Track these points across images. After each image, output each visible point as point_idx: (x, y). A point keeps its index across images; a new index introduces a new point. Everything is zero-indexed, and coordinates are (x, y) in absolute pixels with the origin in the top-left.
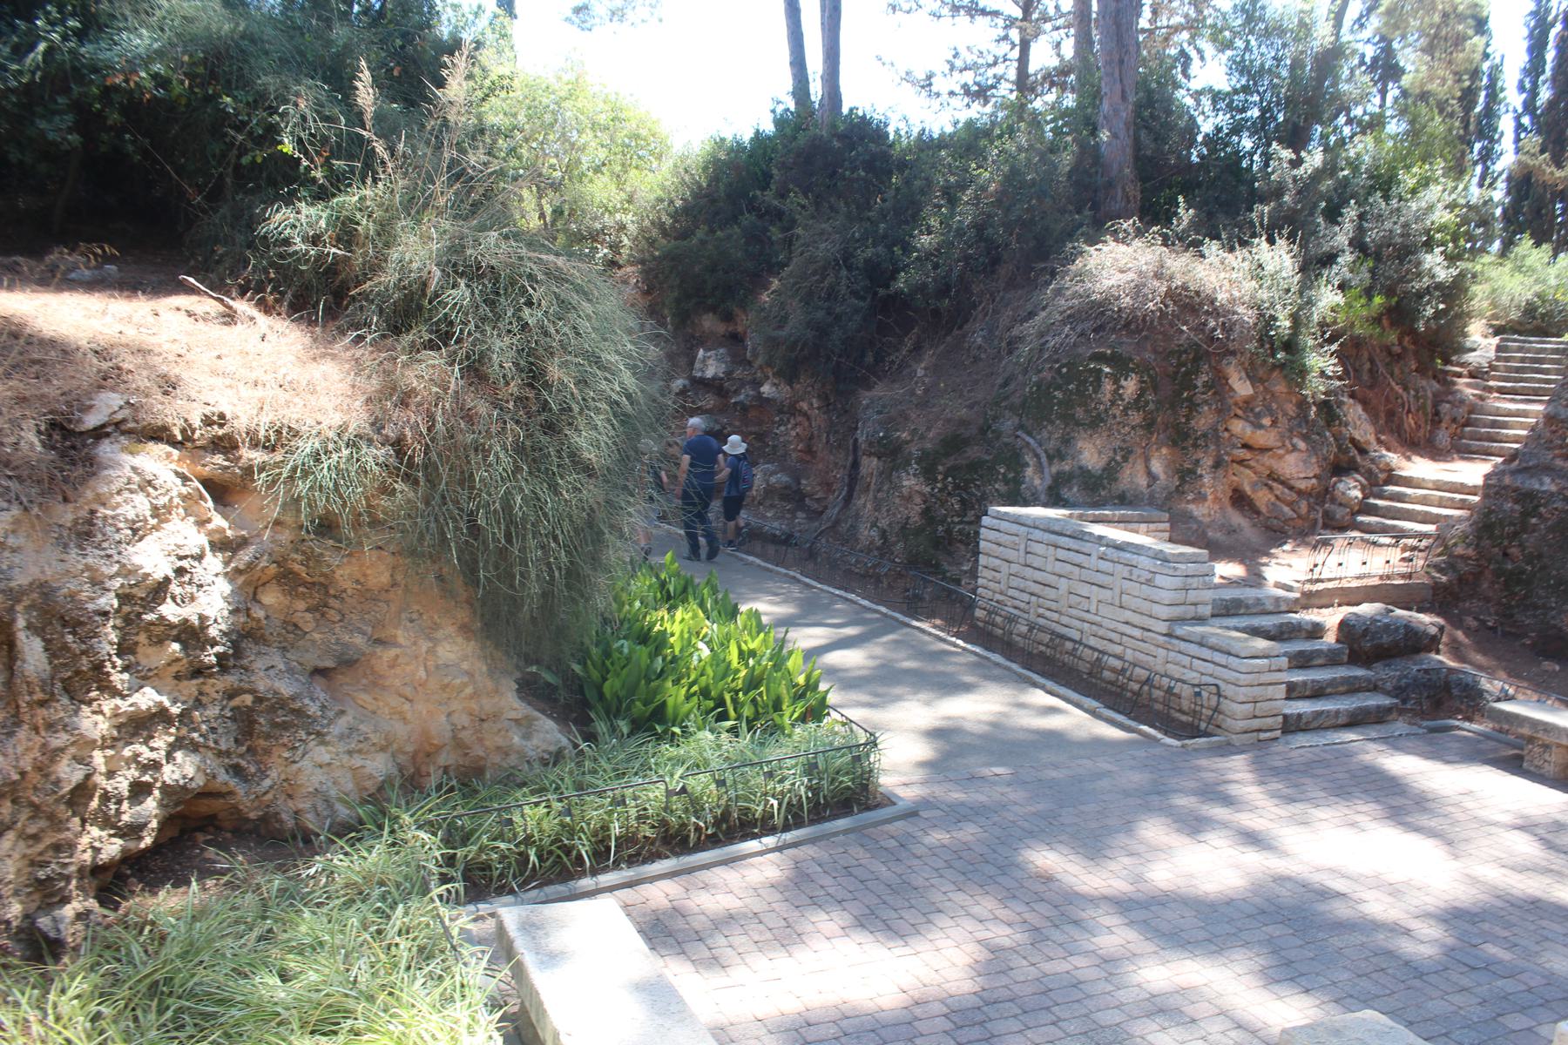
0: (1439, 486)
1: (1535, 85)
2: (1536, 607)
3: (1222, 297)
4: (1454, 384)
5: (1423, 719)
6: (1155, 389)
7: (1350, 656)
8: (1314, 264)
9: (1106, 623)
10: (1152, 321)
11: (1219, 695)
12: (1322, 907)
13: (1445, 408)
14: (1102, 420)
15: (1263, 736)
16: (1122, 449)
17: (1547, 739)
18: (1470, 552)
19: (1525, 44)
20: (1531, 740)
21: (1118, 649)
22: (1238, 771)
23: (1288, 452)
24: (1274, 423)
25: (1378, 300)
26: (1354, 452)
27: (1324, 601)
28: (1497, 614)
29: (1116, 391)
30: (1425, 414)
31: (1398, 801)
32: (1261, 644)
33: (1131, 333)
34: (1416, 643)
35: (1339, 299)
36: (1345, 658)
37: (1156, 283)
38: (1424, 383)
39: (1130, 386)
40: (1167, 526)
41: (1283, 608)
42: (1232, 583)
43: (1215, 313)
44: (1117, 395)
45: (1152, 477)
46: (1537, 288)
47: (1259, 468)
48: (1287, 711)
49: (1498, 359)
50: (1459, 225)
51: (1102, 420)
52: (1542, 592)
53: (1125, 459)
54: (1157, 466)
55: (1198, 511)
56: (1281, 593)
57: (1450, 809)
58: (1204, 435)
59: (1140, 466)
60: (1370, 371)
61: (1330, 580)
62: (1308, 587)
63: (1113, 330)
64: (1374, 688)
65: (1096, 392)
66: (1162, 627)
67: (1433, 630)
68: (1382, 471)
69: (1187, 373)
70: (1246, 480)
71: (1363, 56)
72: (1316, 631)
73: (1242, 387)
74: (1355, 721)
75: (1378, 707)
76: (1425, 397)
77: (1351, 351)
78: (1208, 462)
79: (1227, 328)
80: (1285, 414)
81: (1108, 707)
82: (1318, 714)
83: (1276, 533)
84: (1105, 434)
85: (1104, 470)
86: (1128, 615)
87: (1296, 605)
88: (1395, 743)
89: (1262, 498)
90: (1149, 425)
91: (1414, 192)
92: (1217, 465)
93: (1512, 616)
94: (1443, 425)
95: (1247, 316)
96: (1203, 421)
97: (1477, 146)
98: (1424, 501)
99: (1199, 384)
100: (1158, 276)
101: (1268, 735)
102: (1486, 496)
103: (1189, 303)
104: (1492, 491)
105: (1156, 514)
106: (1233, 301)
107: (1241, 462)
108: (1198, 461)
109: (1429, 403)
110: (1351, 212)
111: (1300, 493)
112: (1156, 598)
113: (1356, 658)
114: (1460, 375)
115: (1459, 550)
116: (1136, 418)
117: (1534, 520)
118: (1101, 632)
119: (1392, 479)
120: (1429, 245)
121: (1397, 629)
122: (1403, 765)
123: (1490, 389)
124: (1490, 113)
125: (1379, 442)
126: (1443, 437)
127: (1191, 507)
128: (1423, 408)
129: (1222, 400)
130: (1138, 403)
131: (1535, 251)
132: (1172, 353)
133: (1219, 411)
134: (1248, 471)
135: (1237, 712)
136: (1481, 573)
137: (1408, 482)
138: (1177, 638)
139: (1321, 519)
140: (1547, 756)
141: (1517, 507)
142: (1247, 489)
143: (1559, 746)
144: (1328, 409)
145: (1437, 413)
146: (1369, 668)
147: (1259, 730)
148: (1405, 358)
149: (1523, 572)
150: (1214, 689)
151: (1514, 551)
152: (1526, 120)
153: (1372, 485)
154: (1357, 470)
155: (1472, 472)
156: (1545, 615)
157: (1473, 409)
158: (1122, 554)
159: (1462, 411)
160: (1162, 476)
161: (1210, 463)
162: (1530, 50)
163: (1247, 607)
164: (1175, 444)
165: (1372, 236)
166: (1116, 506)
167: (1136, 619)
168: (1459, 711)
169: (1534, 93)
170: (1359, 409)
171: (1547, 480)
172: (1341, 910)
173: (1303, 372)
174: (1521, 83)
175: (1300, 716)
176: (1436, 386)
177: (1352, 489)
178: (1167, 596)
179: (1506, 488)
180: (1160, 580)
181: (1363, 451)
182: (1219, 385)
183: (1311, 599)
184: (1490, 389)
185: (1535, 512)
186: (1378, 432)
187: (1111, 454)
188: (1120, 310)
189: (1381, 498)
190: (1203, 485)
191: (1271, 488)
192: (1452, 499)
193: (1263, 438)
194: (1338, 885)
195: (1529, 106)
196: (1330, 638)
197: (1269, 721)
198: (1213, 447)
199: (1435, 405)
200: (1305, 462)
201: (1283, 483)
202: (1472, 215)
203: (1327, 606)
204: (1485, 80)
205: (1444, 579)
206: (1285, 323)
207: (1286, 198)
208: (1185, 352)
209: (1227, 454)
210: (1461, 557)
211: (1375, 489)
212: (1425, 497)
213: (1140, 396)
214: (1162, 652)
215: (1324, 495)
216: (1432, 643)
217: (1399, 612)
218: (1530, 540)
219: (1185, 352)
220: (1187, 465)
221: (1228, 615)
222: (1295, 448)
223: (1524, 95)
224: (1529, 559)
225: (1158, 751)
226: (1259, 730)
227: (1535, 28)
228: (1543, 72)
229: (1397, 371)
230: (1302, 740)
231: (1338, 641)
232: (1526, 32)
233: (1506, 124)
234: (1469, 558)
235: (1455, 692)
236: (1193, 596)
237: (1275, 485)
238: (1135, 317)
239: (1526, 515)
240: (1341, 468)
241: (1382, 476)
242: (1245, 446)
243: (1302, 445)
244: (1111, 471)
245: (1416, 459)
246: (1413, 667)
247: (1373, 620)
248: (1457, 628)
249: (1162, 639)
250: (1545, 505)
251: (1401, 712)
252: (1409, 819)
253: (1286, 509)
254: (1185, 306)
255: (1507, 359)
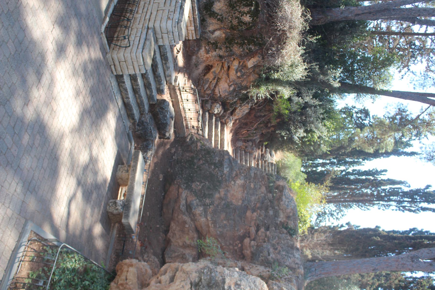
0: (222, 140)
1: (355, 174)
2: (182, 171)
3: (284, 52)
4: (259, 149)
5: (132, 132)
6: (247, 29)
7: (152, 104)
8: (298, 86)
9: (150, 7)
10: (272, 26)
11: (126, 47)
12: (31, 70)
13: (250, 144)
14: (233, 9)
15: (113, 67)
16: (222, 18)
17: (130, 171)
18: (199, 148)
19: (367, 170)
20: (129, 166)
21: (140, 12)
22: (93, 53)
23: (228, 84)
24: (239, 77)
25: (287, 112)
26: (231, 110)
27: (173, 95)
28: (178, 159)
29: (245, 13)
30: (247, 137)
31: (93, 114)
32: (149, 62)
33: (268, 18)
34: (162, 128)
35: (286, 97)
36: (151, 103)
37: (288, 27)
38: (258, 136)
39: (247, 19)
40: (195, 38)
41: (168, 79)
42: (175, 59)
43: (278, 50)
44: (243, 13)
45: (213, 32)
46: (291, 180)
47: (221, 74)
48: (125, 77)
49: (268, 163)
50: (314, 142)
51: (233, 9)
52: (187, 172)
53: (219, 20)
54: (217, 33)
55: (202, 52)
56: (174, 78)
57: (94, 135)
58: (231, 51)
59: (217, 27)
60: (261, 116)
61: (181, 97)
62: (177, 88)
63: (268, 11)
64: (142, 113)
65: (244, 5)
66: (151, 25)
67: (167, 135)
68: (225, 120)
69: (254, 42)
70: (216, 69)
71: (365, 120)
72: (160, 91)
73: (250, 63)
74: (126, 105)
75: (134, 114)
76: (253, 136)
77: (269, 102)
78: (221, 53)
79: (272, 55)
80: (242, 81)
81: (115, 7)
82: (126, 90)
83: (198, 82)
84: (227, 10)
85: (214, 12)
86: (154, 13)
87: (169, 83)
88: (119, 119)
89: (210, 76)
90: (232, 28)
91: (325, 125)
92: (221, 57)
93: (178, 164)
94: (244, 144)
95: (278, 62)
96: (236, 49)
97: (335, 161)
98: (216, 135)
99: (251, 46)
100: (290, 27)
101: (113, 69)
102: (220, 151)
103: (281, 40)
104: (222, 153)
105: (199, 33)
106: (283, 57)
107: (223, 67)
108: (221, 49)
109: (252, 138)
110: (317, 103)
111: (214, 90)
112: (162, 22)
113: (152, 107)
114: (262, 151)
115: (199, 144)
116: (235, 22)
117: (213, 167)
118: (146, 5)
119: (223, 124)
120: (306, 131)
121: (165, 120)
122: (111, 120)
123: (258, 161)
124: (346, 163)
125: (236, 120)
126: (240, 144)
127: (203, 49)
128: (250, 136)
129: (245, 56)
130: (241, 22)
131: (303, 179)
132: (261, 35)
133: (241, 55)
134: (219, 69)
135: (119, 55)
136: (192, 152)
137: (222, 130)
138: (147, 31)
139: (205, 100)
140: (124, 172)
141: (217, 161)
142: (213, 70)
143: (129, 175)
144: (245, 98)
145: (248, 141)
146: (149, 112)
147: (115, 65)
148: (267, 126)
149: (194, 165)
150: (128, 45)
151: (201, 162)
152: (344, 173)
153: (220, 117)
154: (225, 112)
155: (228, 148)
156: (180, 174)
157: (251, 153)
158: (179, 10)
159: (250, 150)
160: (214, 36)
161: (221, 54)
162: (365, 171)
163: (166, 64)
164: (227, 39)
165: (309, 111)
166: (200, 18)
167: (153, 16)
168: (138, 145)
169: (352, 174)
170: (247, 111)
171: (228, 169)
172: (31, 78)
173: (258, 86)
174: (356, 170)
175: (124, 82)
176: (258, 141)
177: (217, 109)
178: (164, 25)
179: (223, 157)
180: (170, 22)
181: (232, 113)
182: (250, 54)
183: (173, 90)
184: (258, 161)
185: (216, 167)
186: (239, 119)
187: (220, 14)
188: (276, 13)
189: (216, 121)
190: (212, 52)
191: (214, 79)
192: (218, 144)
193: (232, 73)
194: (45, 80)
195: (348, 173)
196: (158, 97)
197: (119, 69)
198: (227, 54)
199: (251, 140)
200: (225, 91)
201: (217, 84)
202: (317, 146)
203: (171, 96)
204: (356, 160)
205: (188, 140)
206: (276, 76)
207: (321, 76)
208: (262, 40)
209: (225, 60)
210: (197, 145)
211: (218, 119)
212: (218, 135)
213: (244, 23)
214: (141, 26)
215: (214, 100)
216: (162, 136)
217: (173, 122)
218: (206, 166)
219: (262, 40)
220: (219, 45)
221: (161, 56)
222: (230, 86)
223: (351, 171)
224: (199, 167)
225: (98, 22)
226: (115, 65)
227: (373, 172)
228: (359, 176)
229: (262, 125)
230: (114, 83)
231: (158, 100)
232: (371, 170)
233: (342, 168)
234: (197, 148)
235: (145, 143)
236: (165, 36)
237: (216, 81)
238: (274, 19)
239: (215, 164)
240: (224, 105)
241: (223, 121)
242: (229, 67)
243: (231, 89)
244: (213, 14)
245: (231, 135)
246: (152, 127)
247: (167, 111)
248: (170, 145)
249: (146, 25)
250: (219, 170)
251: (134, 124)
252: (85, 117)
253: (207, 86)
254: (280, 39)
255: (268, 166)
